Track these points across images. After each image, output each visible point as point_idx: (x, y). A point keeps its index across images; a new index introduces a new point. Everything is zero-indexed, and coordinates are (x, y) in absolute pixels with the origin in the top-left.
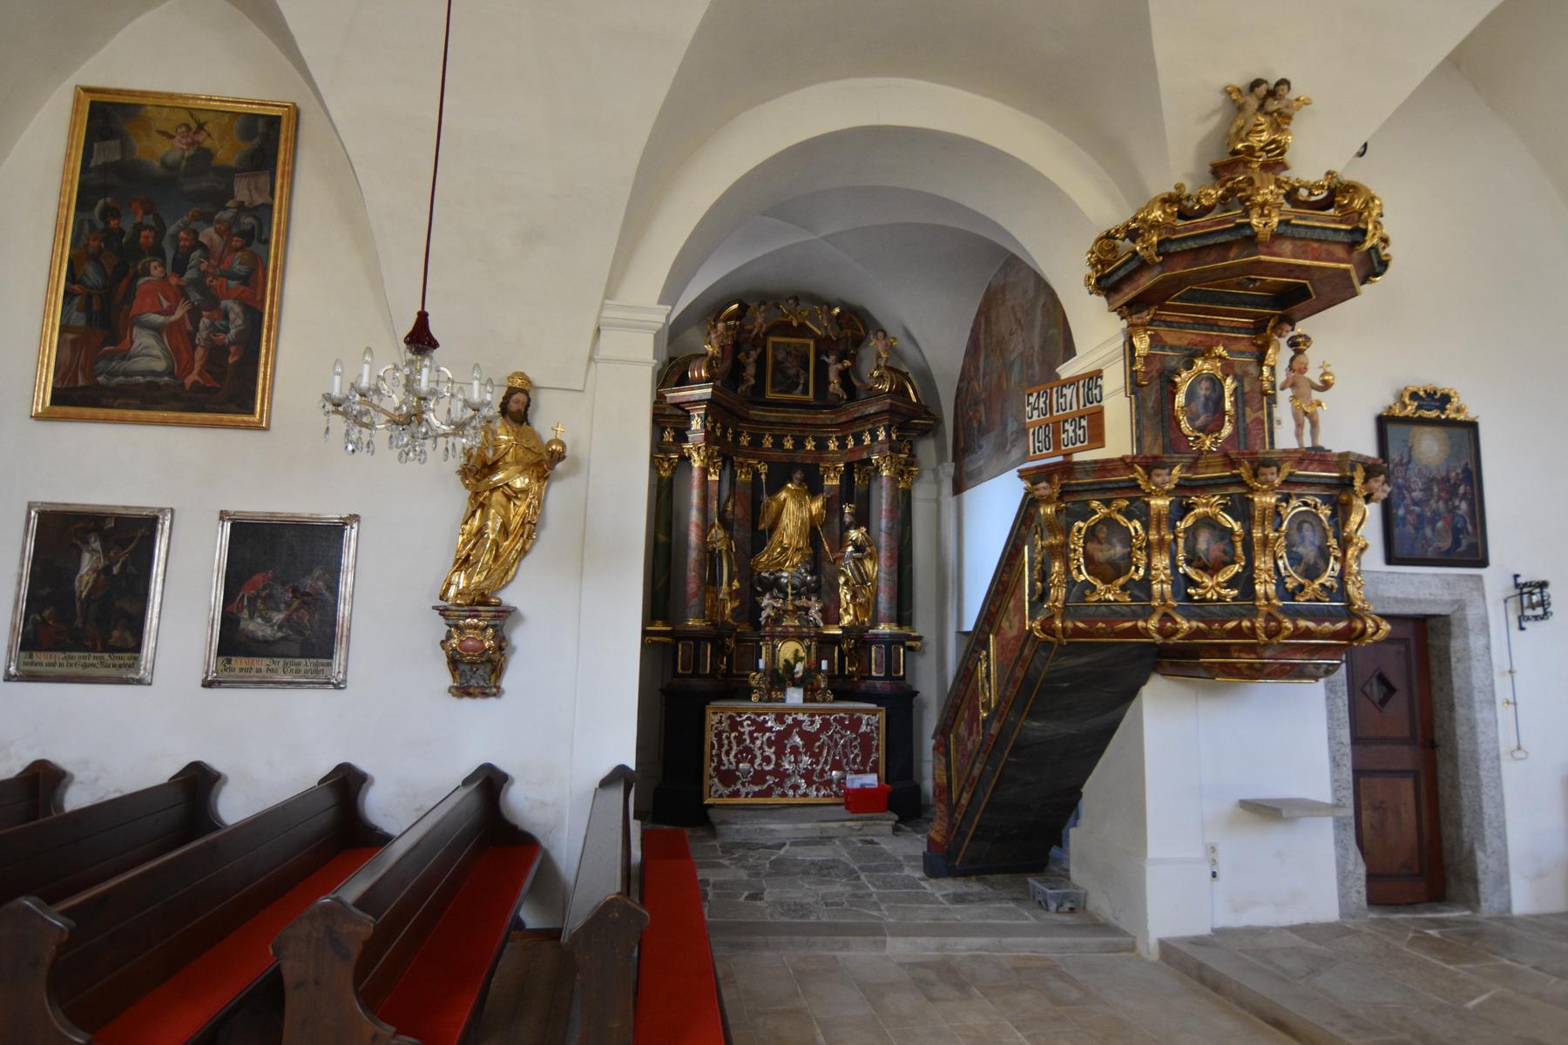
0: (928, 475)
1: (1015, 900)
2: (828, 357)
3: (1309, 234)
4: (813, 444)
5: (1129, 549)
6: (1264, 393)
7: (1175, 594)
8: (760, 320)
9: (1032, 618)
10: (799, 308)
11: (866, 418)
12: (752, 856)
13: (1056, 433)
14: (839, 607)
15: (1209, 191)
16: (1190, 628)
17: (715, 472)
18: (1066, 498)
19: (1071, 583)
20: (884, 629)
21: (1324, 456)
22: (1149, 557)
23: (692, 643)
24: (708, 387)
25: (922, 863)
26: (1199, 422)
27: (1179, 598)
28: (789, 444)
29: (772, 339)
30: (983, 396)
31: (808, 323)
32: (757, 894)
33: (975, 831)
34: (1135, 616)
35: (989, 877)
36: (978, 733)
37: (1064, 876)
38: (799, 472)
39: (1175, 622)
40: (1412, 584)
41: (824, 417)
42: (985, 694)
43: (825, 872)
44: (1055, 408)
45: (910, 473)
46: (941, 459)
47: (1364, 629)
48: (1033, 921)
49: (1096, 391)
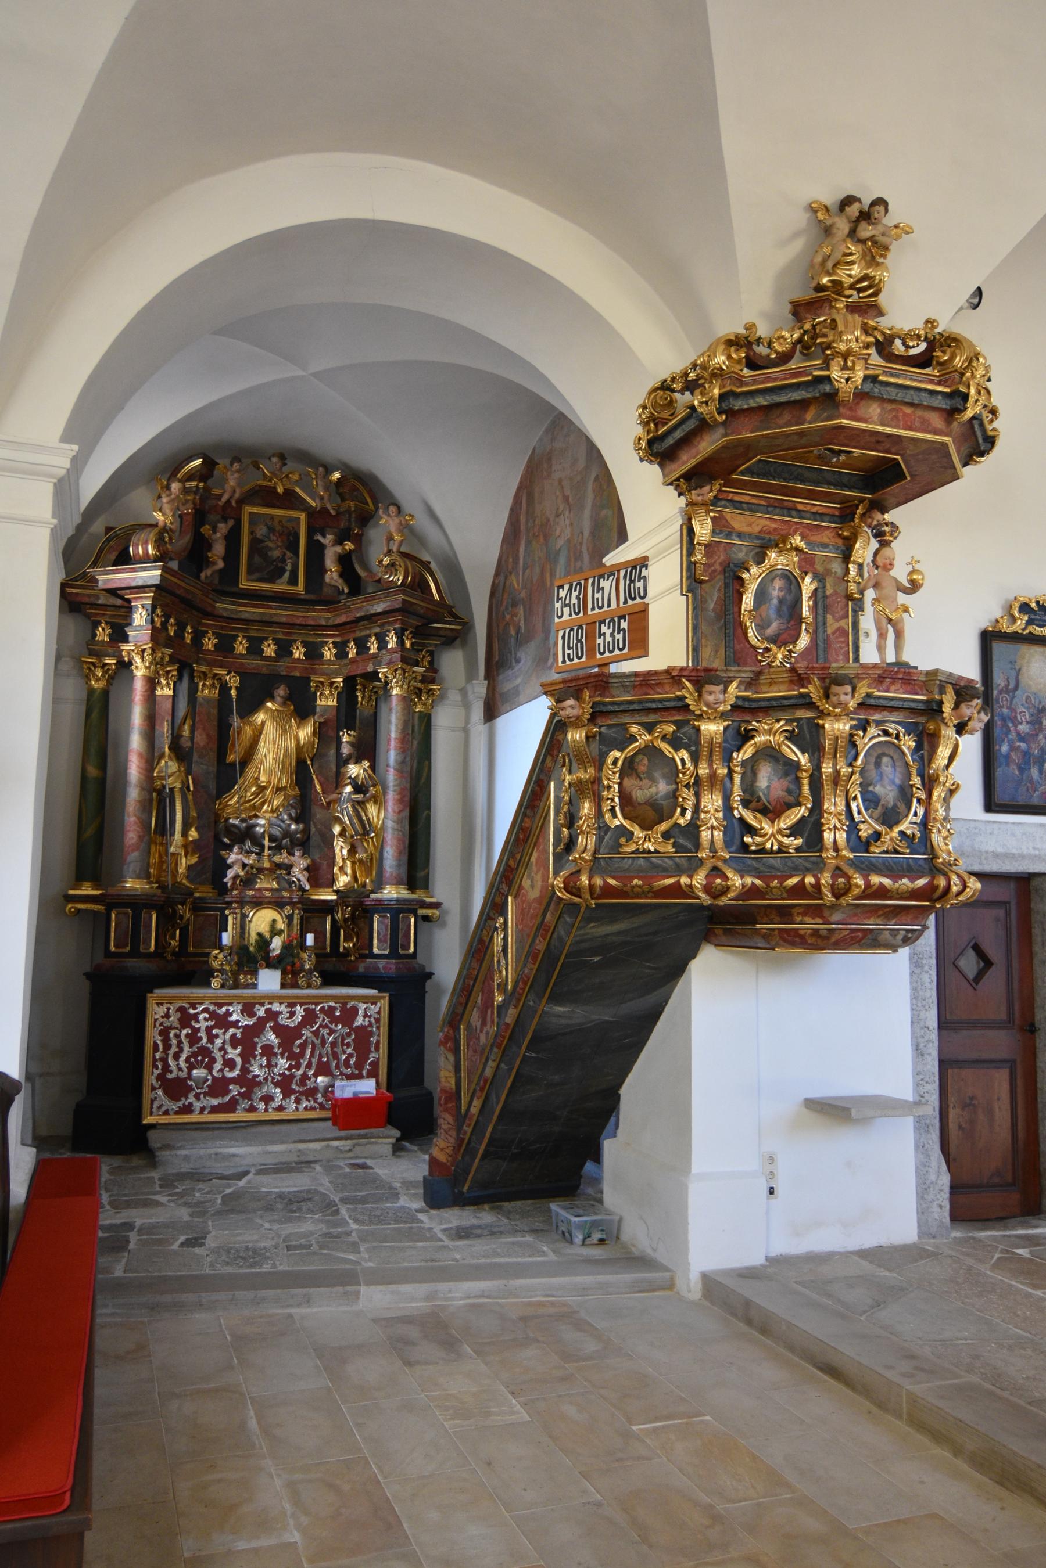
0: (454, 696)
1: (533, 1231)
2: (324, 536)
3: (900, 395)
4: (303, 650)
5: (674, 786)
6: (849, 597)
7: (727, 844)
8: (232, 483)
9: (556, 873)
10: (285, 469)
11: (371, 618)
12: (200, 1190)
13: (591, 637)
14: (334, 865)
15: (783, 333)
16: (744, 886)
17: (168, 684)
18: (600, 721)
19: (603, 829)
20: (391, 892)
21: (909, 673)
22: (698, 796)
23: (130, 911)
24: (155, 568)
25: (422, 1191)
26: (770, 631)
27: (733, 849)
28: (269, 650)
29: (248, 509)
30: (523, 595)
31: (298, 490)
32: (196, 1239)
33: (487, 1146)
34: (679, 871)
35: (506, 1204)
36: (493, 1022)
37: (595, 1200)
38: (282, 687)
39: (725, 878)
40: (1013, 835)
41: (318, 615)
42: (501, 972)
43: (294, 1207)
44: (590, 606)
45: (430, 692)
46: (471, 676)
47: (948, 888)
48: (552, 1257)
49: (639, 584)
